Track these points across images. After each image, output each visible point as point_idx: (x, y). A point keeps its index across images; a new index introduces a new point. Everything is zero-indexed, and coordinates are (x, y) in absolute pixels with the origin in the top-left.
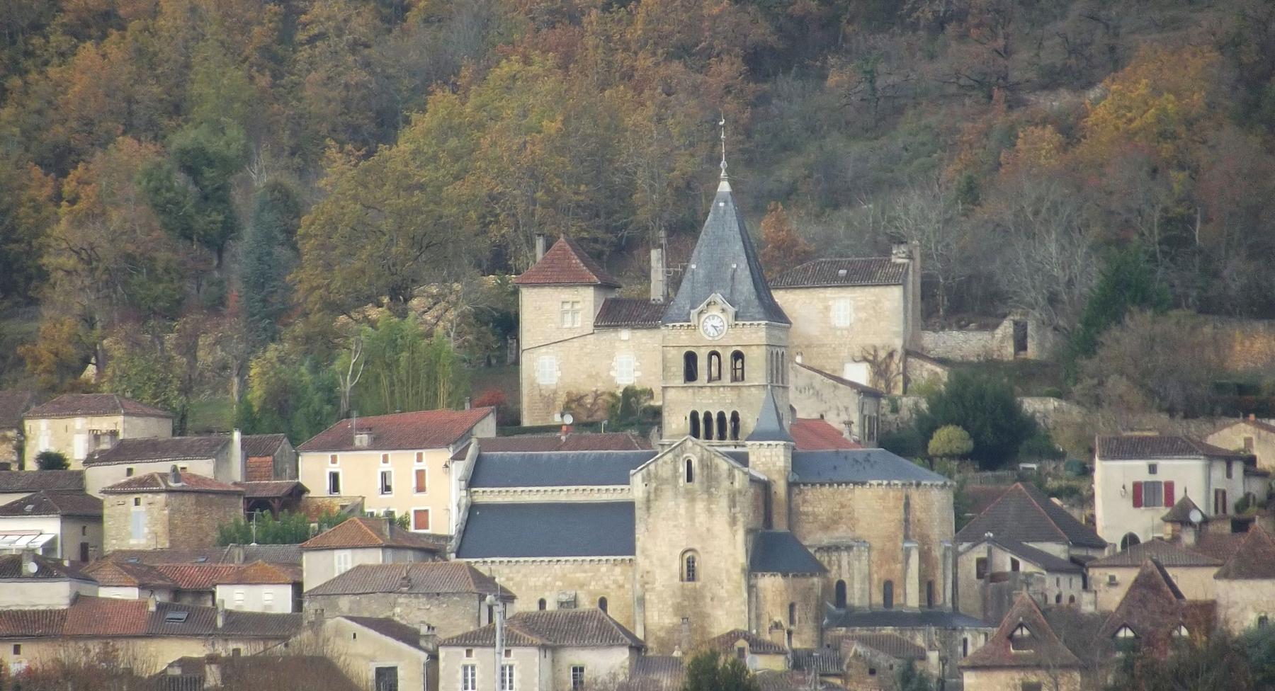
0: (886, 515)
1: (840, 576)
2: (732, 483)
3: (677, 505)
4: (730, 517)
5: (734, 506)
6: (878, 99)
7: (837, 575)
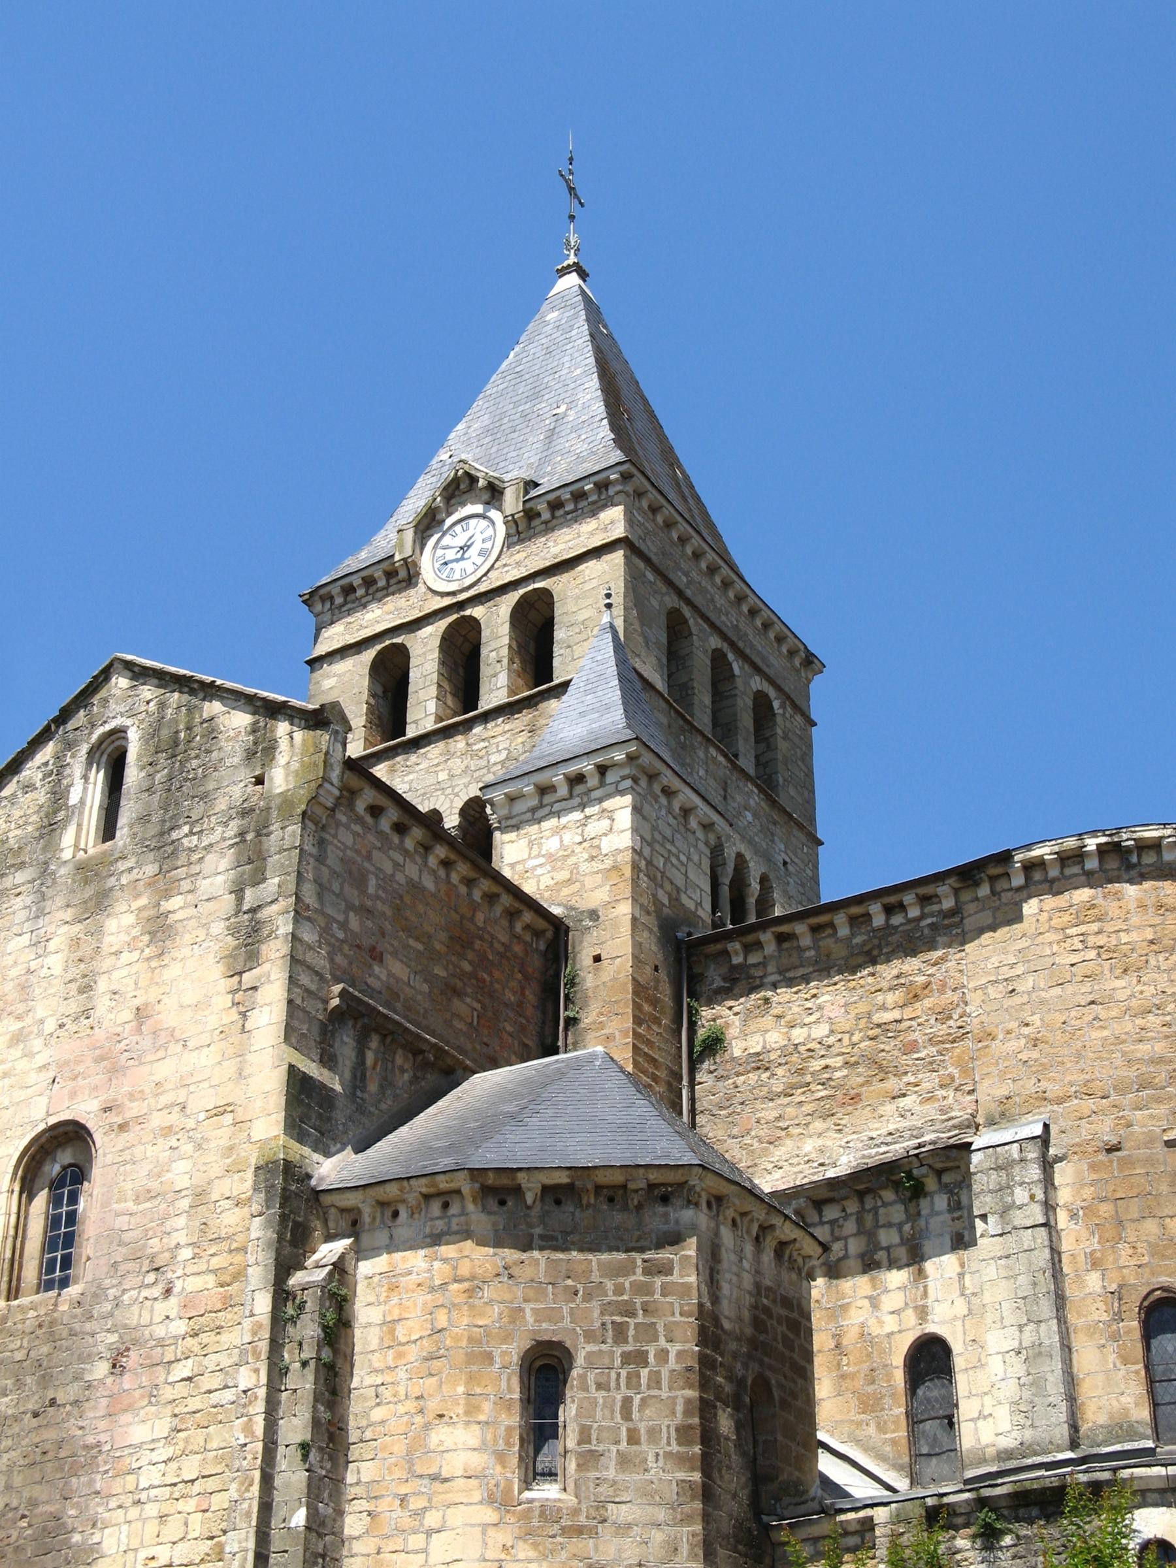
0: (1122, 987)
1: (923, 1313)
2: (259, 781)
3: (40, 944)
4: (234, 931)
5: (258, 878)
6: (42, 1021)
7: (910, 1317)
